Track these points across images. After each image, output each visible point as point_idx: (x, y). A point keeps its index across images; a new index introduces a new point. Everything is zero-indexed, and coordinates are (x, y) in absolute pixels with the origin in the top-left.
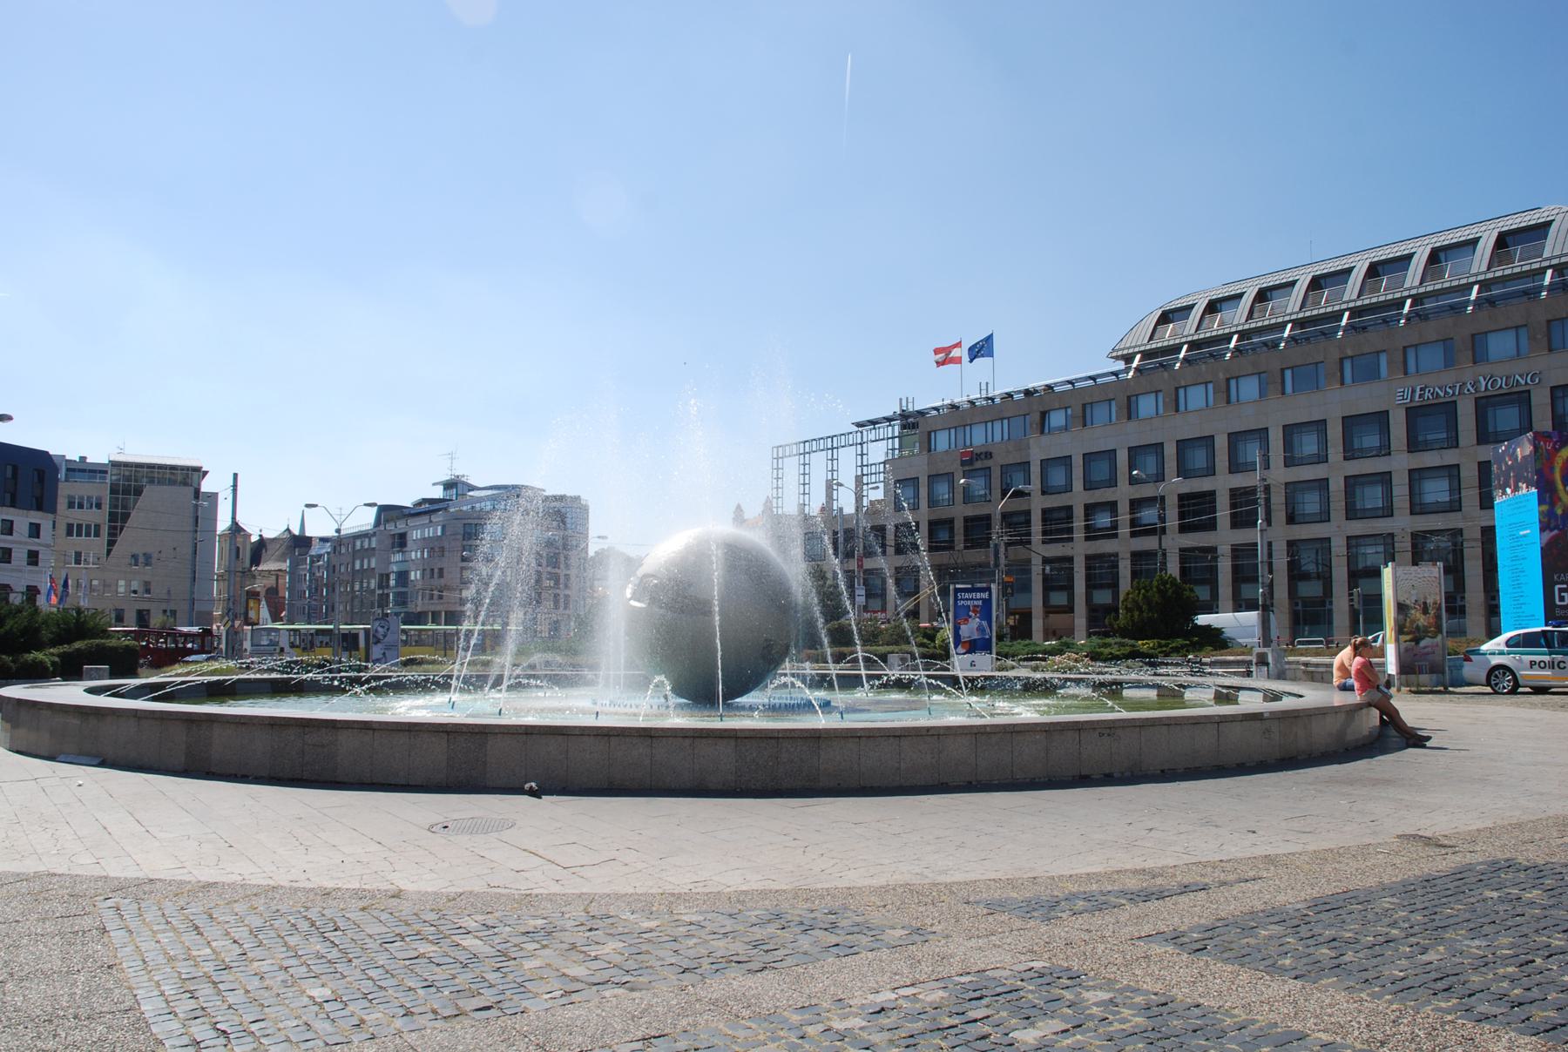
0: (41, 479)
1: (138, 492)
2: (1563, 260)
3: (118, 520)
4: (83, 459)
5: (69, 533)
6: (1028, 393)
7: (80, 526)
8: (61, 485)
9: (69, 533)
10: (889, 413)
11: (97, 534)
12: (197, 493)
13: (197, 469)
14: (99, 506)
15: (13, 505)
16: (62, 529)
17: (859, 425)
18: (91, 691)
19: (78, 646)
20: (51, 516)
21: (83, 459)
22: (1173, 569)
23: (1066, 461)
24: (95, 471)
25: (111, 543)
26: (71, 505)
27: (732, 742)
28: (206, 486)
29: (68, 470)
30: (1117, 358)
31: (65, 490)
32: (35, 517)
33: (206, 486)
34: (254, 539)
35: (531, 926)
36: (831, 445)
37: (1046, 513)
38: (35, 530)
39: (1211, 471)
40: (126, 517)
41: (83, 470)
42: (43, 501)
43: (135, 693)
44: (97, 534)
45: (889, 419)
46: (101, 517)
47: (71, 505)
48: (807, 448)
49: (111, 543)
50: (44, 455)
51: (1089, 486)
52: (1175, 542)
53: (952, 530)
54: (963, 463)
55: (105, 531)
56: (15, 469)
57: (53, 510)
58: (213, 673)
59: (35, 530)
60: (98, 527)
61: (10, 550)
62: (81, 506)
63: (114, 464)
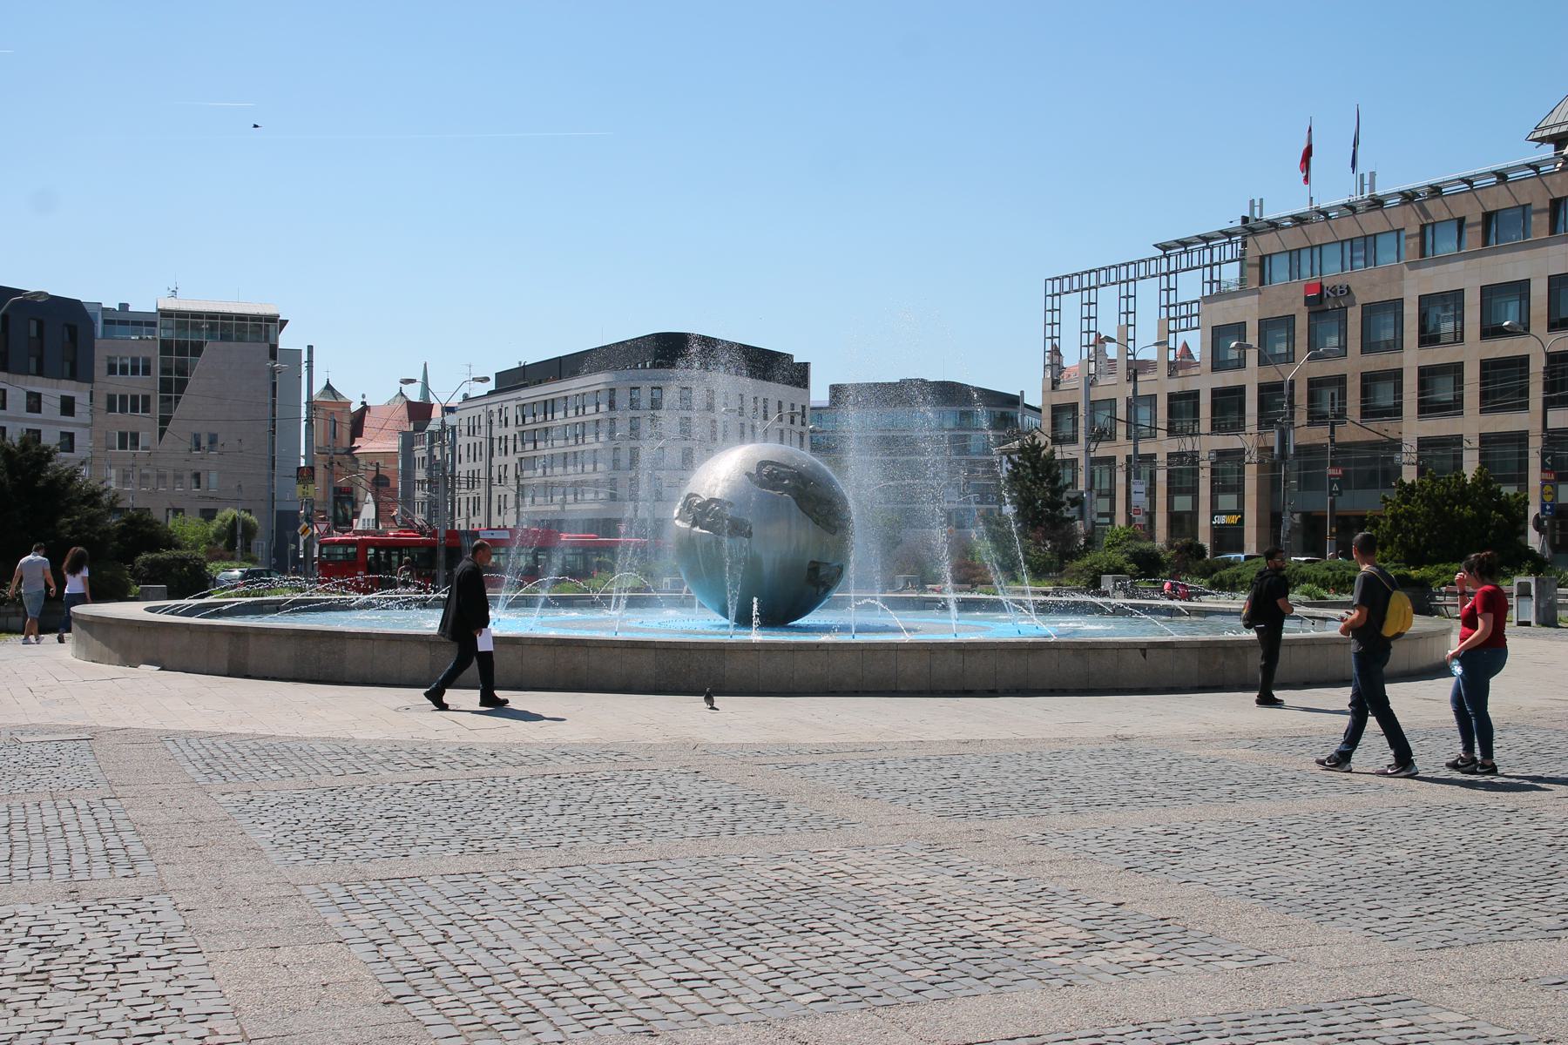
0: (73, 332)
1: (197, 349)
2: (1563, 129)
3: (173, 386)
4: (124, 306)
5: (111, 407)
6: (1502, 176)
7: (123, 398)
8: (98, 344)
9: (111, 407)
10: (1226, 226)
11: (146, 409)
12: (273, 352)
13: (273, 319)
14: (147, 371)
15: (40, 373)
16: (102, 402)
17: (1164, 247)
18: (151, 610)
19: (130, 552)
20: (87, 386)
21: (124, 306)
22: (1471, 465)
23: (1239, 329)
24: (142, 322)
25: (165, 421)
26: (112, 370)
27: (653, 653)
28: (285, 341)
29: (106, 322)
30: (1542, 140)
31: (103, 350)
32: (68, 388)
33: (285, 341)
34: (355, 407)
35: (272, 753)
36: (1124, 275)
37: (1487, 367)
38: (68, 406)
39: (1524, 328)
40: (182, 385)
41: (122, 320)
42: (78, 369)
43: (191, 612)
44: (146, 409)
45: (1228, 234)
46: (147, 386)
47: (112, 370)
48: (1059, 286)
49: (165, 421)
50: (74, 306)
51: (1368, 347)
52: (1472, 424)
53: (1399, 389)
54: (1308, 301)
55: (155, 405)
56: (40, 325)
57: (89, 378)
58: (861, 629)
59: (68, 406)
60: (146, 399)
61: (39, 432)
62: (124, 371)
63: (165, 314)
